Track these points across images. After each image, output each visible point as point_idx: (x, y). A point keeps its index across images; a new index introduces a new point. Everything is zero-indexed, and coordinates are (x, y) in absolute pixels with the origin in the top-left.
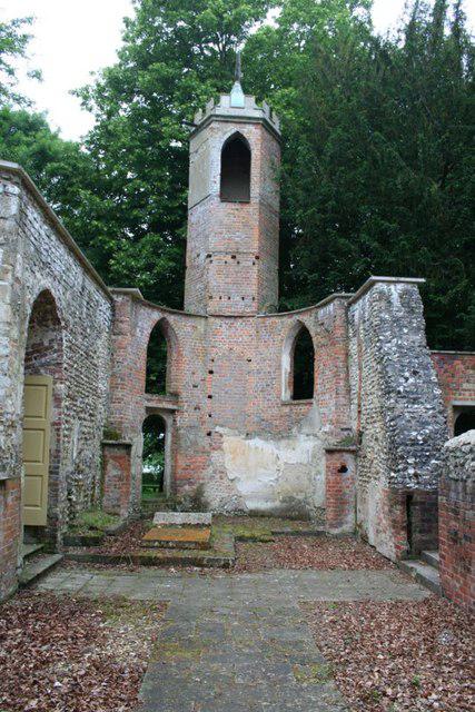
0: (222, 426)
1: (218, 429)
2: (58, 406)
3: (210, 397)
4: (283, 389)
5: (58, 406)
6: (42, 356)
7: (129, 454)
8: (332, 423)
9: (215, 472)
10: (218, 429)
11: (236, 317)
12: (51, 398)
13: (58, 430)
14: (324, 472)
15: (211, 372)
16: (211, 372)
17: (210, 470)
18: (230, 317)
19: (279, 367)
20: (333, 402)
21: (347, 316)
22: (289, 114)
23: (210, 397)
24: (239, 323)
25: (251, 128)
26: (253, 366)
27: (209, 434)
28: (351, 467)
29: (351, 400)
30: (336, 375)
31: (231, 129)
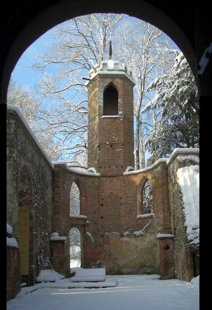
0: (108, 232)
1: (106, 233)
2: (31, 220)
3: (102, 218)
4: (138, 211)
5: (31, 220)
6: (23, 197)
7: (63, 246)
8: (162, 226)
9: (106, 255)
10: (106, 233)
11: (113, 176)
12: (28, 216)
13: (31, 231)
14: (159, 251)
15: (102, 205)
16: (102, 205)
17: (104, 254)
18: (111, 176)
19: (136, 201)
20: (162, 215)
21: (167, 172)
22: (137, 180)
23: (102, 218)
24: (115, 179)
25: (118, 80)
26: (123, 200)
27: (102, 236)
28: (171, 247)
29: (170, 213)
30: (163, 202)
31: (109, 81)
